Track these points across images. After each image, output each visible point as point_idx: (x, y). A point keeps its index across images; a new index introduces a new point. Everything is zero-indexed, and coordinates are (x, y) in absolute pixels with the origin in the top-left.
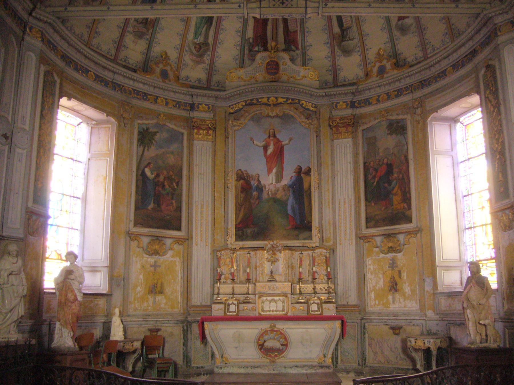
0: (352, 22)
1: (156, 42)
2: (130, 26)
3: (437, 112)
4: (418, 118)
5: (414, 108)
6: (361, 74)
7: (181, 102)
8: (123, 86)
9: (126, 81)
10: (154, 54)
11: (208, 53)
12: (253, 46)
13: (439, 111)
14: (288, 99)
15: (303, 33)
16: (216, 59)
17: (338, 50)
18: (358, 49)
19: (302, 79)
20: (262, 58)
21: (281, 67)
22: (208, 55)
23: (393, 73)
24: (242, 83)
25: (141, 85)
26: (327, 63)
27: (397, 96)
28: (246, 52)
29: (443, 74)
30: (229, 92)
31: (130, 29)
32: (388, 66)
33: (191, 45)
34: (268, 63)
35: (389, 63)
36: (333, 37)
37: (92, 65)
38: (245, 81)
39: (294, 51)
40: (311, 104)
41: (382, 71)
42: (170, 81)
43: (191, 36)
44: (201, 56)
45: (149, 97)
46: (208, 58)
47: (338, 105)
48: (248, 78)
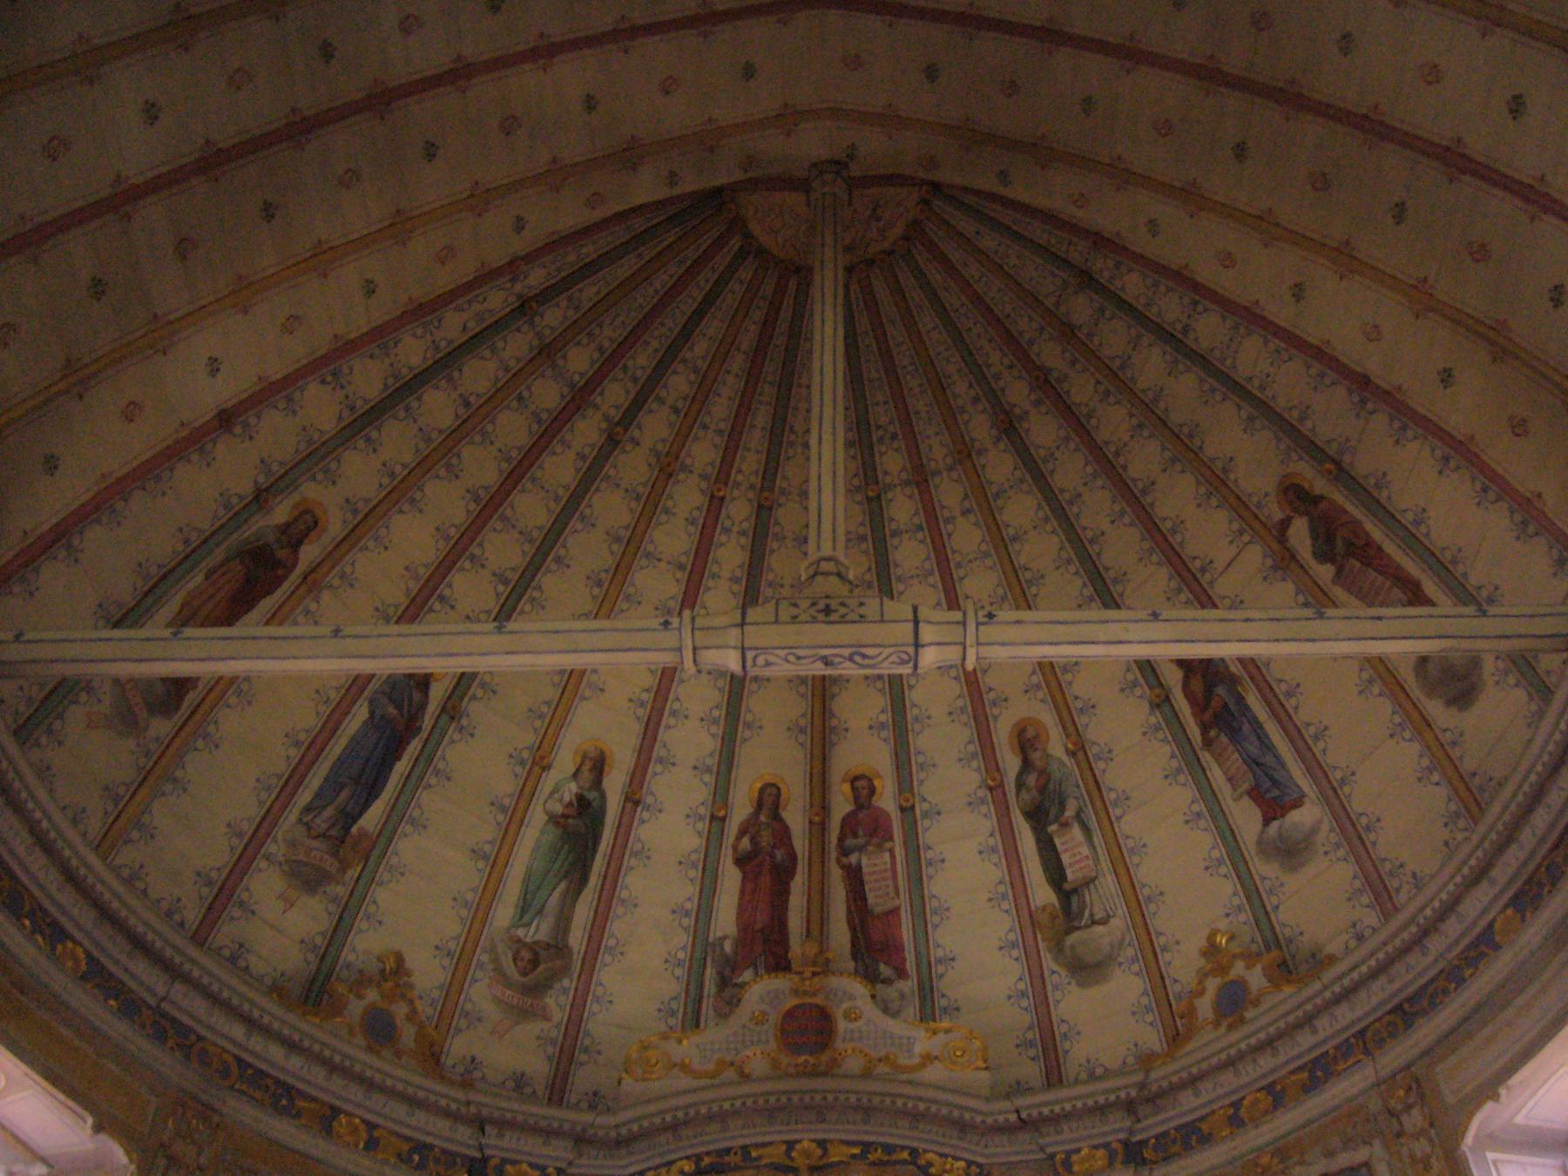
0: (1097, 860)
1: (368, 917)
2: (280, 836)
3: (1495, 1097)
4: (1421, 1147)
5: (1391, 1113)
6: (1153, 1039)
7: (431, 1147)
8: (201, 1038)
9: (219, 1020)
10: (351, 957)
11: (566, 982)
12: (733, 970)
13: (1503, 1091)
14: (867, 1147)
15: (920, 917)
16: (592, 1007)
17: (1056, 968)
18: (1130, 952)
19: (923, 1065)
20: (763, 992)
21: (842, 1025)
22: (565, 991)
23: (1275, 1005)
24: (686, 1082)
25: (276, 1052)
26: (1019, 1017)
27: (1310, 1087)
28: (710, 987)
29: (1484, 944)
30: (629, 1114)
31: (275, 848)
32: (1256, 979)
33: (501, 948)
34: (790, 1014)
35: (1258, 969)
36: (1030, 920)
37: (87, 917)
38: (697, 1075)
39: (888, 982)
40: (962, 1164)
41: (1233, 1002)
42: (398, 1054)
43: (503, 914)
44: (536, 990)
45: (301, 1103)
46: (562, 999)
47: (1075, 1158)
48: (711, 1067)
